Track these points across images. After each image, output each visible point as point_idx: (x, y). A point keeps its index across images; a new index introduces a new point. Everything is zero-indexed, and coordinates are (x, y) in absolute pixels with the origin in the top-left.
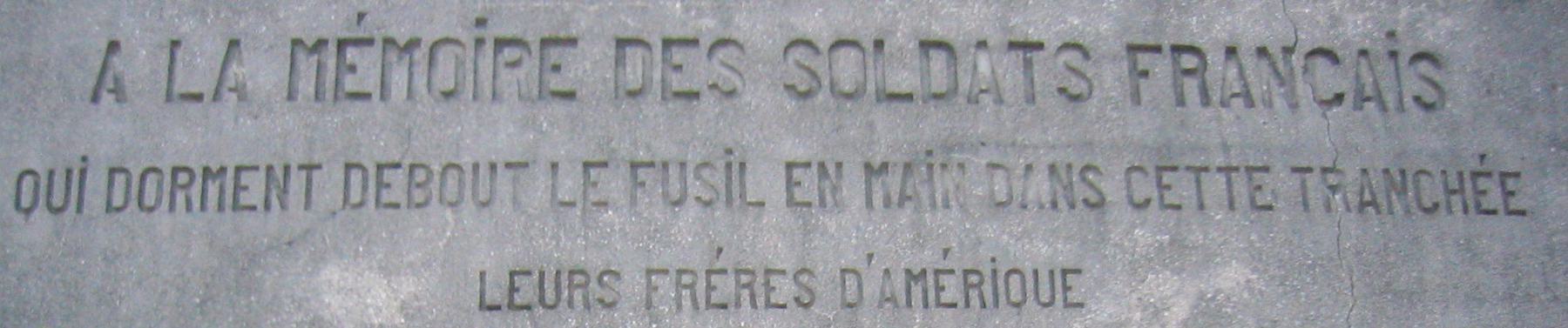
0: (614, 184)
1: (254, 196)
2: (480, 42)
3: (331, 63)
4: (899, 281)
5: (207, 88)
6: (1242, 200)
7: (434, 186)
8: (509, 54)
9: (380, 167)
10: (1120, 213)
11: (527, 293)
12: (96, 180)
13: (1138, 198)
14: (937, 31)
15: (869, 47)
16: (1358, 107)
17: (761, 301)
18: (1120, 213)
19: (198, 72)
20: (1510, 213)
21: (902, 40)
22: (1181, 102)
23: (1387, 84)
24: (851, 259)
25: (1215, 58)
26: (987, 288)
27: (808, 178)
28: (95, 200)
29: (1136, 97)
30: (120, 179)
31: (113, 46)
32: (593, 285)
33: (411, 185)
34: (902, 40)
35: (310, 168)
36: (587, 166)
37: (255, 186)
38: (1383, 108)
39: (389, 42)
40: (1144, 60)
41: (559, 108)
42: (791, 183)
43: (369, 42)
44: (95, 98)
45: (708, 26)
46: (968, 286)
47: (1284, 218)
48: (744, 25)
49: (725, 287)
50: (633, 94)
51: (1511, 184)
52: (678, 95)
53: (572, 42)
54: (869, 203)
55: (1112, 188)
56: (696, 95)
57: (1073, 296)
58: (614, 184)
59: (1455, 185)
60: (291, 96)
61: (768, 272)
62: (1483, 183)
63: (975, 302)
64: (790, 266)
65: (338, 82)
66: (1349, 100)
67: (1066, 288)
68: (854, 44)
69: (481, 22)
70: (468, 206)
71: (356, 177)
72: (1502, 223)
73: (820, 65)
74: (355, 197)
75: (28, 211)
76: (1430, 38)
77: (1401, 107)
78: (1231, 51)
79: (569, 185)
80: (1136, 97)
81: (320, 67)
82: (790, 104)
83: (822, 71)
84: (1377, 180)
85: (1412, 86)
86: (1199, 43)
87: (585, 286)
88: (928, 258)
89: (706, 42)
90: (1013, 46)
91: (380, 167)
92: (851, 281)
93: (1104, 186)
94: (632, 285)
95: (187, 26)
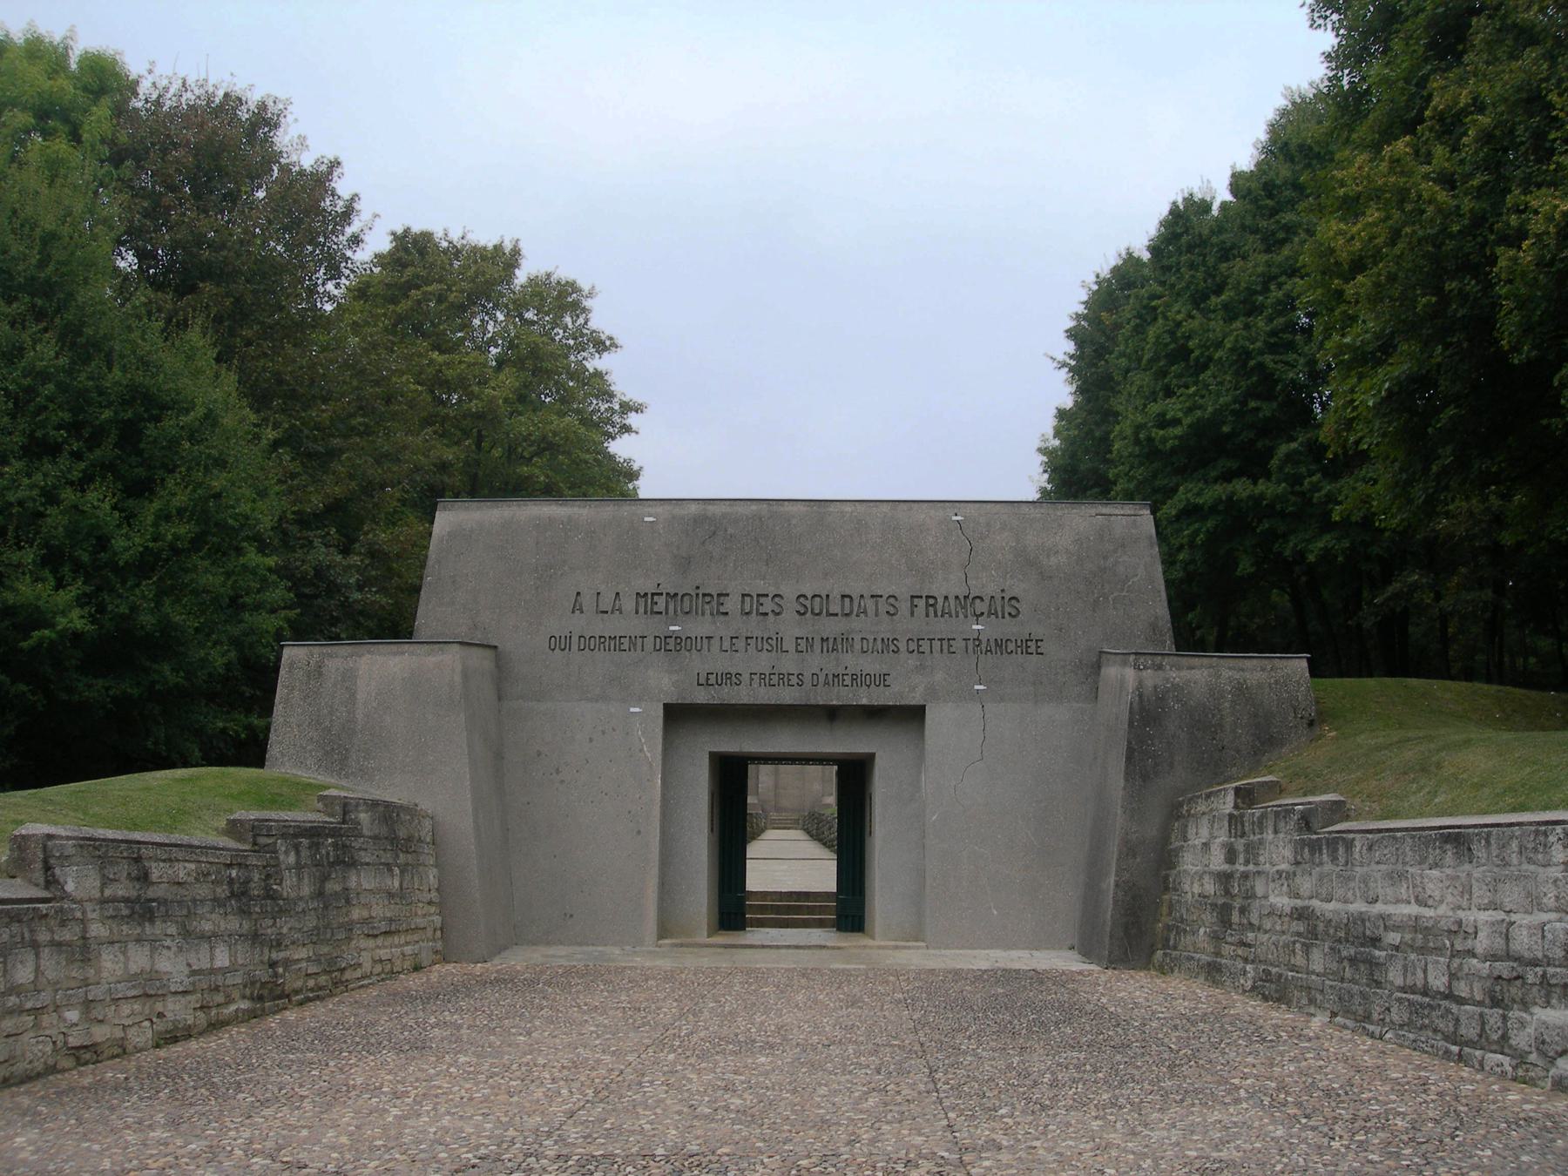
0: (740, 644)
1: (625, 646)
2: (697, 595)
3: (649, 601)
4: (830, 677)
5: (610, 610)
6: (945, 651)
7: (683, 644)
8: (708, 599)
9: (666, 637)
10: (903, 654)
11: (712, 680)
12: (575, 639)
13: (911, 649)
14: (847, 593)
15: (825, 597)
16: (989, 616)
17: (945, 651)
18: (903, 654)
19: (607, 602)
20: (1038, 654)
21: (836, 595)
22: (927, 615)
23: (999, 609)
24: (816, 671)
25: (940, 601)
26: (859, 680)
27: (803, 643)
28: (575, 647)
29: (912, 614)
30: (582, 639)
31: (578, 594)
32: (733, 678)
33: (676, 644)
34: (836, 595)
35: (709, 638)
36: (732, 638)
37: (626, 641)
38: (997, 617)
39: (668, 594)
40: (916, 600)
41: (722, 618)
42: (798, 645)
43: (662, 594)
44: (573, 612)
45: (772, 591)
46: (853, 679)
47: (421, 528)
48: (783, 590)
49: (775, 679)
50: (747, 613)
51: (1039, 644)
52: (762, 614)
53: (728, 595)
54: (822, 651)
55: (902, 646)
56: (767, 614)
57: (887, 683)
58: (740, 644)
59: (1019, 644)
60: (637, 612)
61: (789, 674)
62: (1029, 643)
63: (855, 684)
64: (796, 673)
65: (652, 609)
66: (986, 614)
67: (885, 680)
68: (819, 596)
69: (698, 588)
70: (694, 651)
71: (658, 640)
72: (1035, 657)
73: (808, 603)
74: (658, 648)
75: (553, 650)
76: (1016, 592)
77: (1003, 617)
78: (946, 598)
79: (726, 645)
80: (912, 614)
81: (646, 602)
82: (797, 617)
83: (809, 606)
84: (992, 644)
85: (1008, 609)
86: (935, 595)
87: (730, 678)
88: (841, 670)
89: (771, 596)
90: (872, 596)
91: (666, 637)
92: (815, 677)
93: (899, 645)
94: (745, 677)
95: (602, 588)
